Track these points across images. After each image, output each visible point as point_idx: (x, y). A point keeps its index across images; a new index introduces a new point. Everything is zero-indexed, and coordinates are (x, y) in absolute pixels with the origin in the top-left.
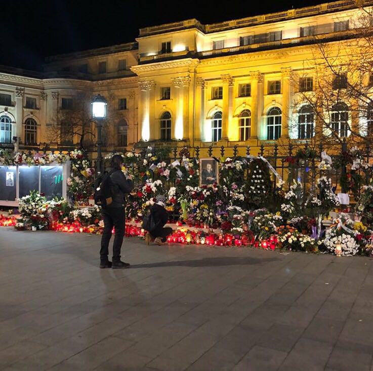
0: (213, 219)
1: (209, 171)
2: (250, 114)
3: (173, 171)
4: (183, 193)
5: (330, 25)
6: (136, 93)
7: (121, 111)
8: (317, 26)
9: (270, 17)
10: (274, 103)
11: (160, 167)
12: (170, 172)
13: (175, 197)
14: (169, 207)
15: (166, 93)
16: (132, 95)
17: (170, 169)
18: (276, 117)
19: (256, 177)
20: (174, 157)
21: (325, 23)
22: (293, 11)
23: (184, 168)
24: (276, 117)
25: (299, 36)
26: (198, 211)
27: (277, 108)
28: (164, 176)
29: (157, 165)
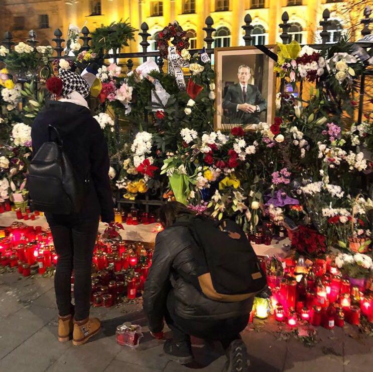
0: (261, 216)
1: (244, 87)
2: (196, 34)
3: (143, 89)
4: (173, 149)
6: (60, 7)
7: (43, 29)
10: (221, 22)
11: (105, 76)
12: (134, 92)
13: (151, 160)
14: (136, 183)
15: (95, 8)
16: (55, 10)
17: (132, 81)
18: (224, 39)
20: (140, 49)
23: (172, 79)
24: (224, 39)
26: (217, 196)
27: (225, 28)
28: (118, 101)
29: (96, 72)
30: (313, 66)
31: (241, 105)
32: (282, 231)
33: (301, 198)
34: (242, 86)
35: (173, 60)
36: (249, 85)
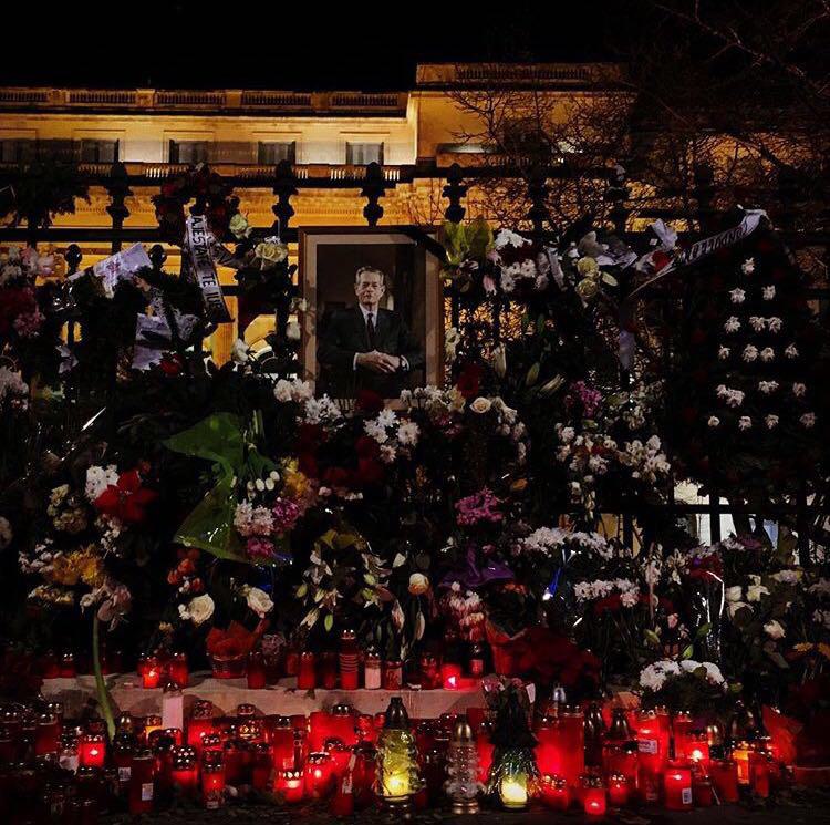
1: (370, 314)
5: (246, 146)
8: (216, 143)
9: (83, 99)
19: (747, 328)
21: (236, 139)
22: (151, 92)
25: (167, 161)
30: (527, 268)
31: (363, 355)
32: (477, 656)
33: (519, 565)
34: (365, 313)
35: (197, 247)
36: (382, 311)
